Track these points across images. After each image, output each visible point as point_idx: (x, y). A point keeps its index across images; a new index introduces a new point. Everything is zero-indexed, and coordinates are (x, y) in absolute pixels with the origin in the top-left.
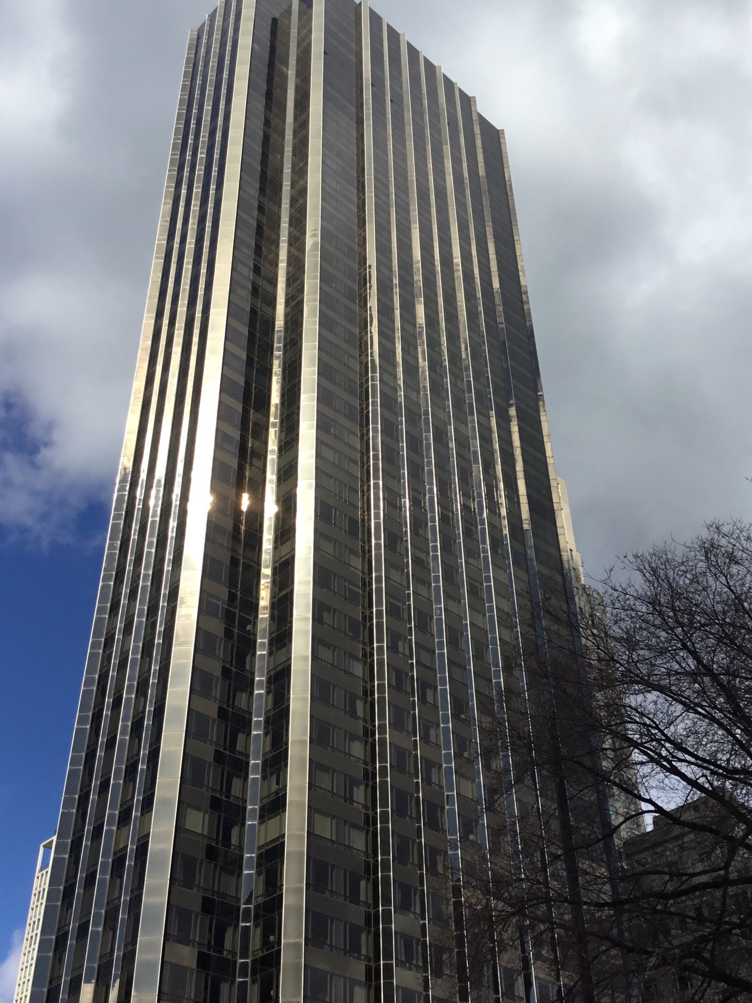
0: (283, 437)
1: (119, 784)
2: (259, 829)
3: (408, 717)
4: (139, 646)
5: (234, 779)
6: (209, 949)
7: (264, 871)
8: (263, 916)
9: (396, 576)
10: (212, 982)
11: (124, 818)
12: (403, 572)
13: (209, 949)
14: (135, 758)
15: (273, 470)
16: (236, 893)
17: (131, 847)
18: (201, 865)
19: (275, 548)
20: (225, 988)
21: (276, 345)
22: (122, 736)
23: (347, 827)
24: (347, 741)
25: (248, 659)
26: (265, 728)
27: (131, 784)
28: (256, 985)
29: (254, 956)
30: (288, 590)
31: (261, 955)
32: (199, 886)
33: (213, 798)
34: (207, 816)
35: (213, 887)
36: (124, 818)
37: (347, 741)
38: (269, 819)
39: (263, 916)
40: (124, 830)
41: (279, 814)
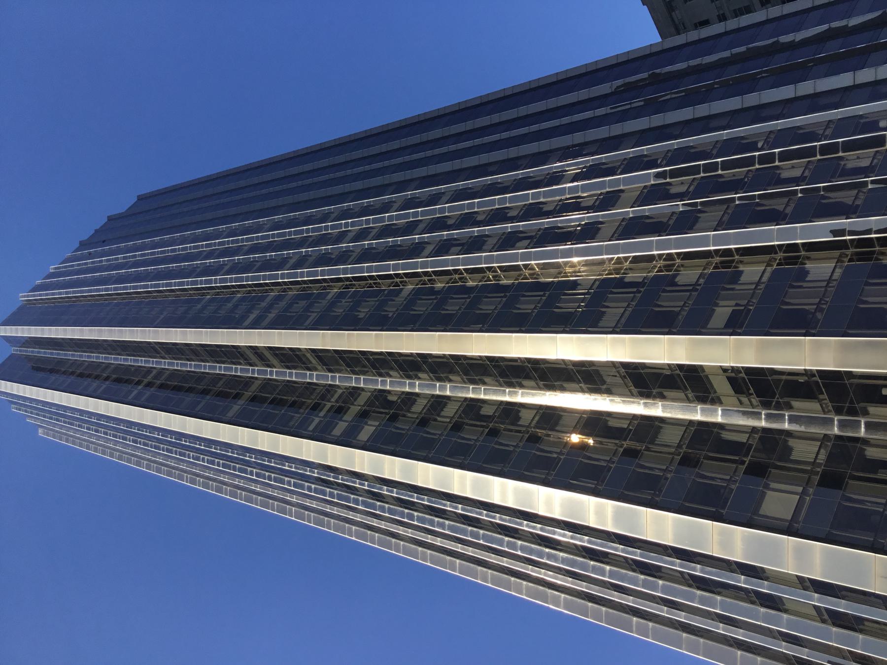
0: (532, 383)
1: (610, 571)
2: (799, 410)
3: (763, 205)
4: (484, 535)
5: (482, 413)
6: (743, 463)
7: (863, 405)
8: (852, 402)
9: (607, 230)
10: (863, 471)
11: (772, 603)
12: (700, 211)
13: (743, 463)
14: (687, 577)
15: (533, 395)
16: (683, 426)
17: (817, 600)
18: (428, 433)
19: (609, 392)
20: (872, 453)
21: (407, 389)
22: (783, 623)
23: (737, 287)
24: (805, 285)
25: (726, 436)
26: (478, 384)
27: (866, 623)
28: (665, 393)
29: (829, 411)
30: (308, 355)
31: (827, 401)
32: (729, 480)
33: (820, 484)
34: (773, 485)
35: (669, 453)
36: (772, 603)
37: (805, 285)
38: (715, 392)
39: (852, 402)
40: (788, 606)
41: (707, 377)
